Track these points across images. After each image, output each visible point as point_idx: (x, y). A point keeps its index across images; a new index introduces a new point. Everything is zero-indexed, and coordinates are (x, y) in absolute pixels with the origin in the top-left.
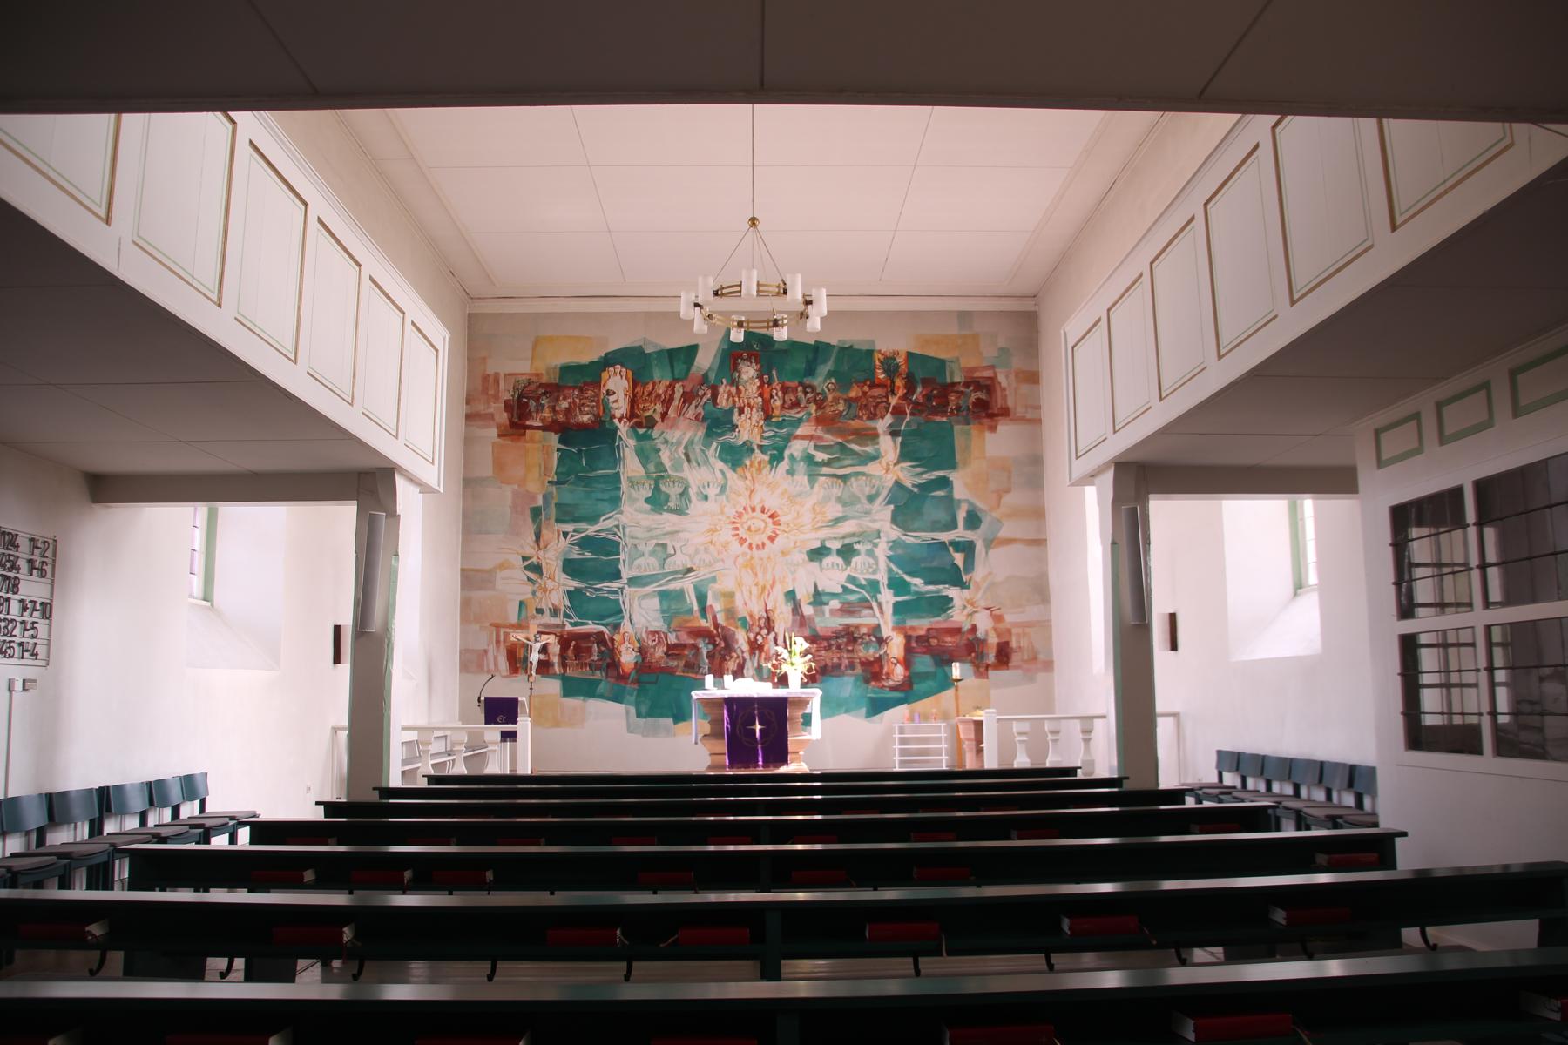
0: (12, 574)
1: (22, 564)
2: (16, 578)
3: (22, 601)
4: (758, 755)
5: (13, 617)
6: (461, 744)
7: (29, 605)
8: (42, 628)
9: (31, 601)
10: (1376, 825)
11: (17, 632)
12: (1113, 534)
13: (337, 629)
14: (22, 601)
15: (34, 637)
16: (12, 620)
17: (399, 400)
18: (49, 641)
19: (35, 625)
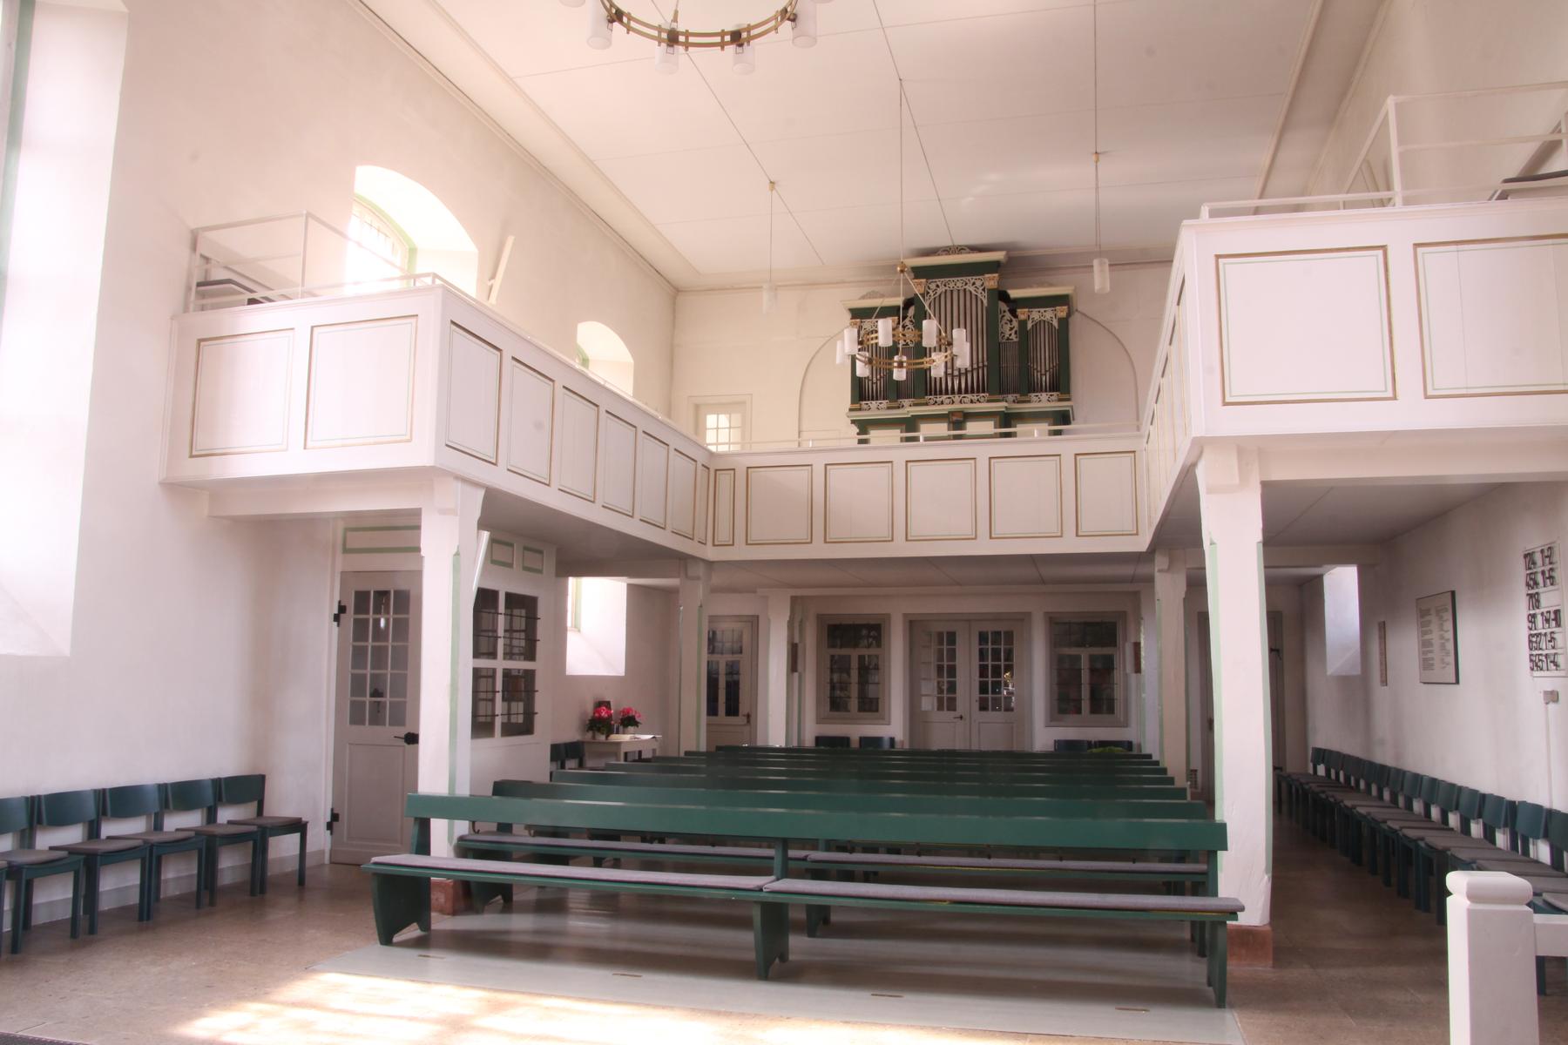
13: (1384, 682)
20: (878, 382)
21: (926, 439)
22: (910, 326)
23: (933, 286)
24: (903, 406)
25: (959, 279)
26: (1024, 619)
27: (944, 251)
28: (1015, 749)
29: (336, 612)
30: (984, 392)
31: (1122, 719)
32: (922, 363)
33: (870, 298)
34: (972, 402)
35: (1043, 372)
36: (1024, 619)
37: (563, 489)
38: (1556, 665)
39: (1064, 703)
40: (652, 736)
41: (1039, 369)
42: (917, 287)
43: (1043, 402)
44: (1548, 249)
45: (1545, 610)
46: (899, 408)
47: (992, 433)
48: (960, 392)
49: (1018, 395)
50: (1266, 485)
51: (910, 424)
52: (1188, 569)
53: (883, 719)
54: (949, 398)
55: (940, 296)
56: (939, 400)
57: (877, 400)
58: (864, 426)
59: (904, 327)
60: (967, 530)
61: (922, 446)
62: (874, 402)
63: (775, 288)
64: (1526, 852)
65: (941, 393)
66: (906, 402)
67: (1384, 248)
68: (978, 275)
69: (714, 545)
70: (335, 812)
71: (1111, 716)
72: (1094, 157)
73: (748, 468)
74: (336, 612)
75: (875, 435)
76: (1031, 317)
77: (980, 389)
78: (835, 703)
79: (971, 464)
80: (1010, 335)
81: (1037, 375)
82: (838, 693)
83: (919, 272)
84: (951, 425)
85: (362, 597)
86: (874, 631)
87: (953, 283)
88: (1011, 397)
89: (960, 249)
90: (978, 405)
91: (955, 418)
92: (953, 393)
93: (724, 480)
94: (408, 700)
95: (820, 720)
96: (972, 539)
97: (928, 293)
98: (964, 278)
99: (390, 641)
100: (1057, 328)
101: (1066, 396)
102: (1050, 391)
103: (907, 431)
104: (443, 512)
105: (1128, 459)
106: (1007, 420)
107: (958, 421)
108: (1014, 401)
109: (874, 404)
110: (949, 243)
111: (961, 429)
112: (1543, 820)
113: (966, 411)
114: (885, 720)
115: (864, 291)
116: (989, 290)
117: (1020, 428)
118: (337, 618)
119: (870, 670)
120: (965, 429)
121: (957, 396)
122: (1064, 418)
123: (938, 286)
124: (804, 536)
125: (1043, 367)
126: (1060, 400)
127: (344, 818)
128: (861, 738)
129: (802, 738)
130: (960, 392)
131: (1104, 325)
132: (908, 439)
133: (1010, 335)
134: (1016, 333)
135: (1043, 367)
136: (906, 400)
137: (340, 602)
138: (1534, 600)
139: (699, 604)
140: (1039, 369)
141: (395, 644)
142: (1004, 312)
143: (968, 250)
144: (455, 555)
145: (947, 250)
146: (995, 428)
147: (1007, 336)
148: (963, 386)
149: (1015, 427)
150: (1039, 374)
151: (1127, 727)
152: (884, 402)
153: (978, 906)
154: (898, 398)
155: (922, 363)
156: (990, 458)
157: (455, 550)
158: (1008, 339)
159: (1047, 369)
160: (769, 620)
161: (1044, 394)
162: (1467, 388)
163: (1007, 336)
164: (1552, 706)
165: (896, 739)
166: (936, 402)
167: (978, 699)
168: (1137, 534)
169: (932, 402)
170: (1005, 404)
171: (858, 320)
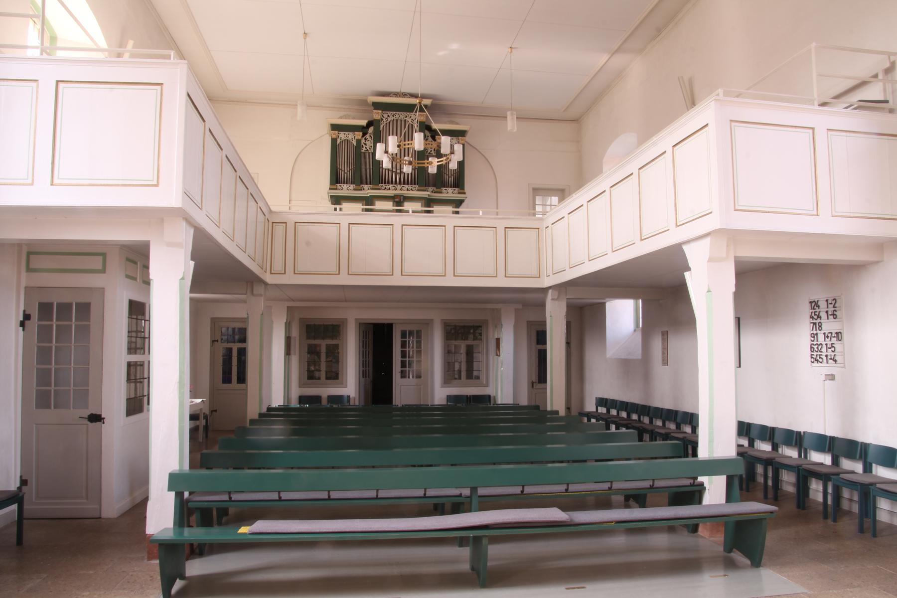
0: (818, 321)
1: (823, 315)
2: (820, 322)
3: (824, 334)
4: (347, 414)
5: (820, 342)
6: (334, 362)
7: (829, 335)
8: (838, 346)
9: (829, 333)
10: (403, 375)
11: (824, 349)
12: (149, 357)
13: (665, 362)
14: (824, 334)
15: (833, 352)
16: (821, 344)
17: (796, 127)
18: (844, 352)
19: (834, 345)
20: (348, 172)
21: (413, 212)
22: (369, 139)
23: (386, 116)
24: (364, 189)
25: (403, 113)
26: (428, 323)
27: (395, 94)
28: (422, 403)
29: (22, 319)
30: (415, 184)
31: (484, 383)
32: (424, 163)
33: (345, 119)
34: (408, 190)
35: (450, 176)
36: (428, 323)
37: (224, 232)
38: (835, 361)
39: (451, 375)
40: (201, 400)
41: (447, 174)
42: (377, 115)
43: (450, 193)
44: (885, 140)
45: (827, 332)
46: (361, 190)
47: (420, 210)
48: (400, 183)
49: (435, 188)
50: (735, 257)
51: (369, 201)
52: (567, 299)
53: (342, 384)
54: (394, 186)
55: (389, 122)
56: (387, 187)
57: (347, 183)
58: (336, 200)
59: (366, 139)
60: (439, 269)
61: (410, 216)
62: (345, 185)
63: (309, 106)
64: (806, 457)
65: (388, 183)
66: (366, 187)
67: (813, 129)
68: (397, 111)
69: (271, 273)
70: (24, 478)
71: (478, 380)
72: (509, 50)
73: (296, 222)
74: (22, 319)
75: (346, 206)
76: (340, 137)
77: (413, 182)
78: (311, 376)
79: (337, 226)
80: (431, 151)
81: (446, 177)
82: (312, 368)
83: (377, 106)
84: (395, 203)
85: (45, 309)
86: (334, 330)
87: (398, 115)
88: (430, 189)
89: (404, 95)
90: (411, 192)
91: (397, 200)
92: (396, 183)
93: (279, 229)
94: (89, 388)
95: (301, 385)
96: (494, 277)
97: (382, 119)
98: (405, 113)
99: (54, 343)
100: (355, 145)
101: (462, 191)
102: (453, 187)
103: (366, 205)
104: (170, 245)
105: (535, 232)
106: (429, 202)
107: (399, 201)
108: (432, 192)
109: (345, 186)
110: (398, 90)
111: (401, 206)
112: (828, 442)
113: (405, 195)
114: (344, 385)
115: (342, 113)
116: (420, 122)
117: (435, 208)
118: (22, 324)
119: (335, 355)
120: (403, 206)
121: (399, 186)
122: (458, 203)
123: (388, 116)
124: (334, 269)
125: (450, 173)
126: (459, 193)
127: (33, 482)
128: (328, 396)
129: (290, 397)
130: (400, 183)
131: (480, 150)
132: (367, 210)
133: (431, 151)
134: (434, 150)
135: (450, 173)
136: (366, 186)
137: (24, 311)
138: (817, 326)
139: (261, 313)
140: (343, 170)
141: (58, 345)
142: (428, 136)
143: (409, 96)
144: (181, 279)
145: (396, 94)
146: (422, 207)
147: (429, 151)
148: (402, 180)
149: (433, 207)
150: (447, 176)
151: (487, 386)
152: (352, 185)
153: (644, 523)
154: (361, 183)
155: (424, 163)
156: (454, 226)
157: (181, 276)
158: (430, 153)
159: (452, 174)
160: (273, 322)
161: (450, 189)
162: (850, 213)
163: (429, 151)
164: (828, 382)
165: (351, 396)
166: (386, 188)
167: (400, 371)
168: (539, 277)
169: (383, 188)
170: (428, 193)
171: (337, 132)
